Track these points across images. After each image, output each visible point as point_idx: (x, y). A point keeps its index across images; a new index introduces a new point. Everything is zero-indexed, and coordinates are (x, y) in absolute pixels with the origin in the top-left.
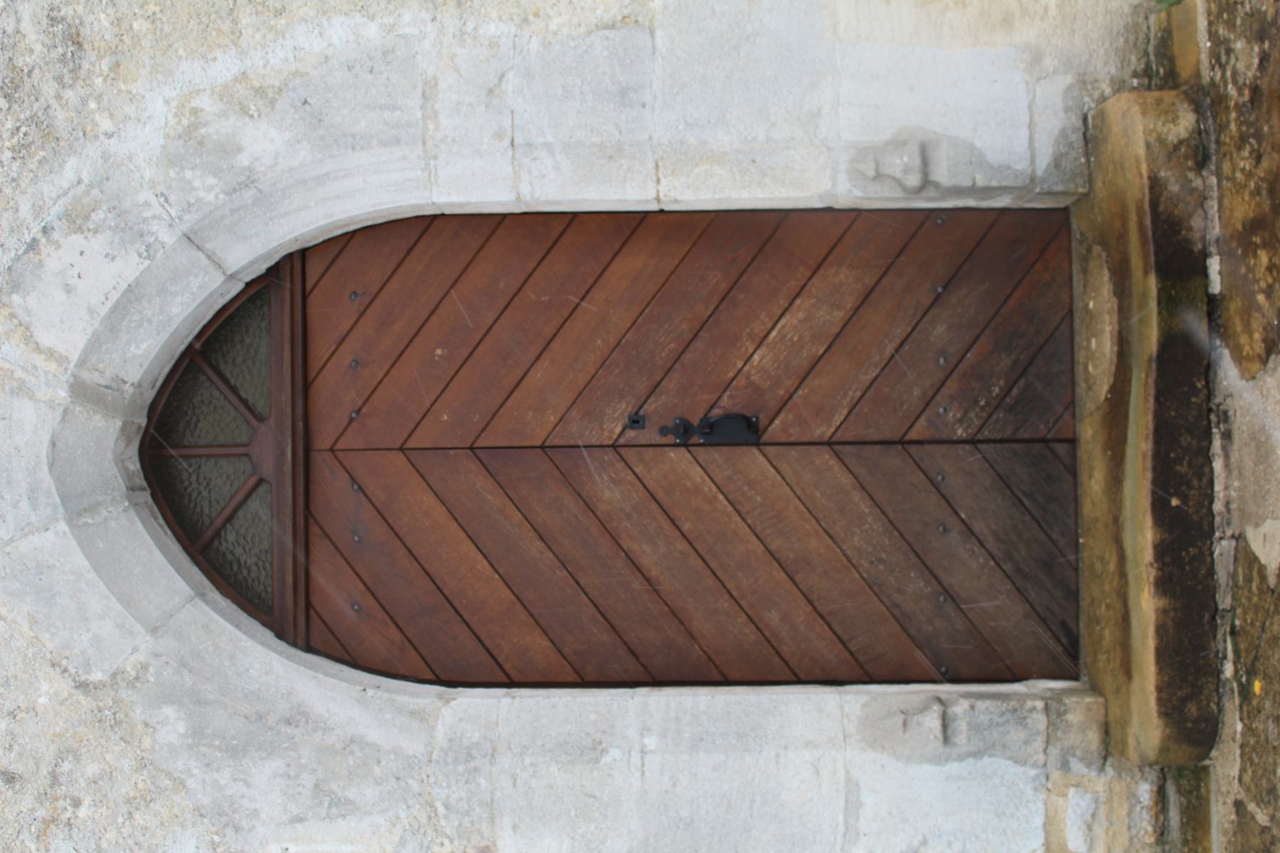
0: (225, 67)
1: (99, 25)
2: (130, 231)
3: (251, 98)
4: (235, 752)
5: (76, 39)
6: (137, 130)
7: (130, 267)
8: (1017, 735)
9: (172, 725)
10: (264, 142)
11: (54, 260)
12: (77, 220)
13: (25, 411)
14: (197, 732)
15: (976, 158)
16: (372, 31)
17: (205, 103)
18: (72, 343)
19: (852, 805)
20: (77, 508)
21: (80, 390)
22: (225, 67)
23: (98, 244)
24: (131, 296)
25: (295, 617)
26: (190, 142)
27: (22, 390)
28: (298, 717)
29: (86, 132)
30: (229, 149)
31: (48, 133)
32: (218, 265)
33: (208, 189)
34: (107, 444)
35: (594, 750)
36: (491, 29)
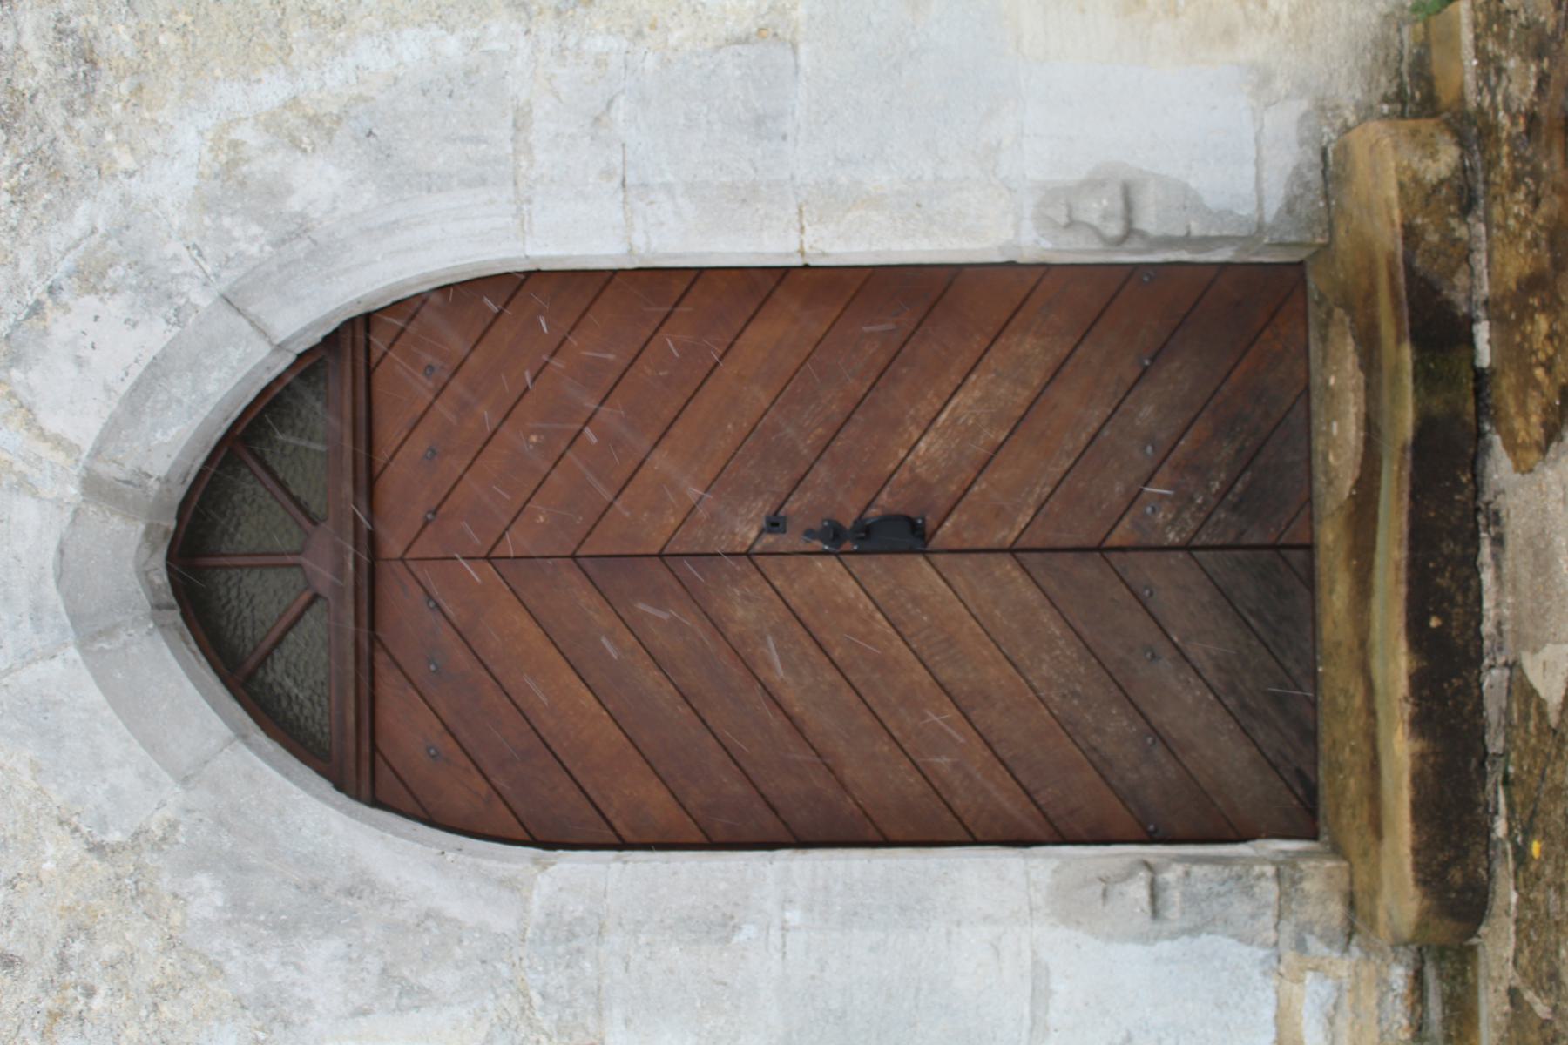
0: (272, 90)
1: (118, 38)
2: (156, 290)
3: (305, 128)
4: (285, 929)
5: (88, 58)
6: (165, 166)
7: (155, 335)
8: (1241, 908)
9: (207, 896)
10: (319, 183)
11: (61, 327)
12: (90, 277)
13: (27, 512)
14: (238, 906)
15: (1190, 201)
16: (452, 46)
17: (247, 134)
18: (85, 428)
19: (1040, 994)
20: (90, 631)
21: (93, 486)
22: (272, 90)
23: (116, 307)
24: (157, 371)
25: (361, 766)
26: (230, 182)
27: (23, 485)
28: (361, 886)
29: (102, 170)
30: (275, 191)
33: (251, 240)
34: (127, 553)
35: (723, 927)
36: (598, 44)
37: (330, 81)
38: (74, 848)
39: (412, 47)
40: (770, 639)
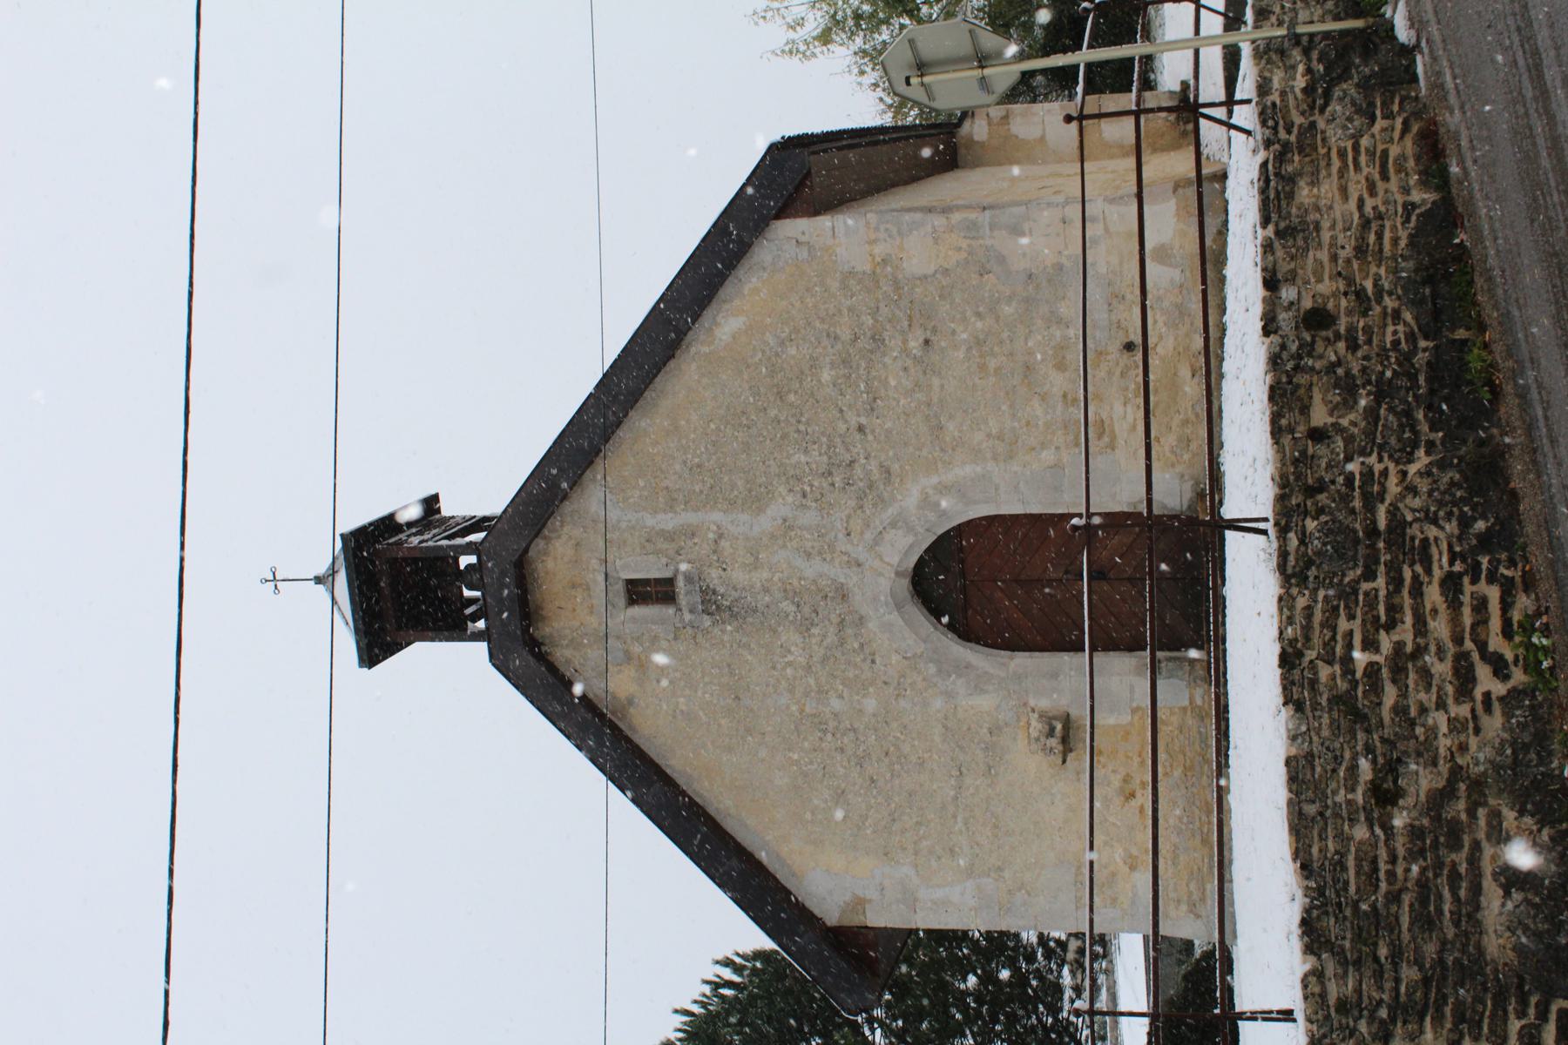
0: (934, 480)
1: (896, 467)
2: (910, 529)
3: (943, 489)
5: (888, 472)
6: (910, 498)
7: (911, 539)
9: (932, 669)
12: (893, 525)
13: (882, 580)
14: (940, 671)
15: (1165, 507)
16: (979, 469)
17: (931, 492)
18: (895, 560)
20: (899, 607)
21: (898, 574)
22: (934, 480)
23: (900, 532)
25: (965, 632)
26: (926, 503)
27: (881, 574)
28: (968, 666)
30: (938, 504)
31: (883, 501)
32: (1267, 1016)
35: (1054, 675)
36: (1015, 468)
37: (949, 477)
38: (899, 657)
39: (968, 469)
40: (1359, 24)
